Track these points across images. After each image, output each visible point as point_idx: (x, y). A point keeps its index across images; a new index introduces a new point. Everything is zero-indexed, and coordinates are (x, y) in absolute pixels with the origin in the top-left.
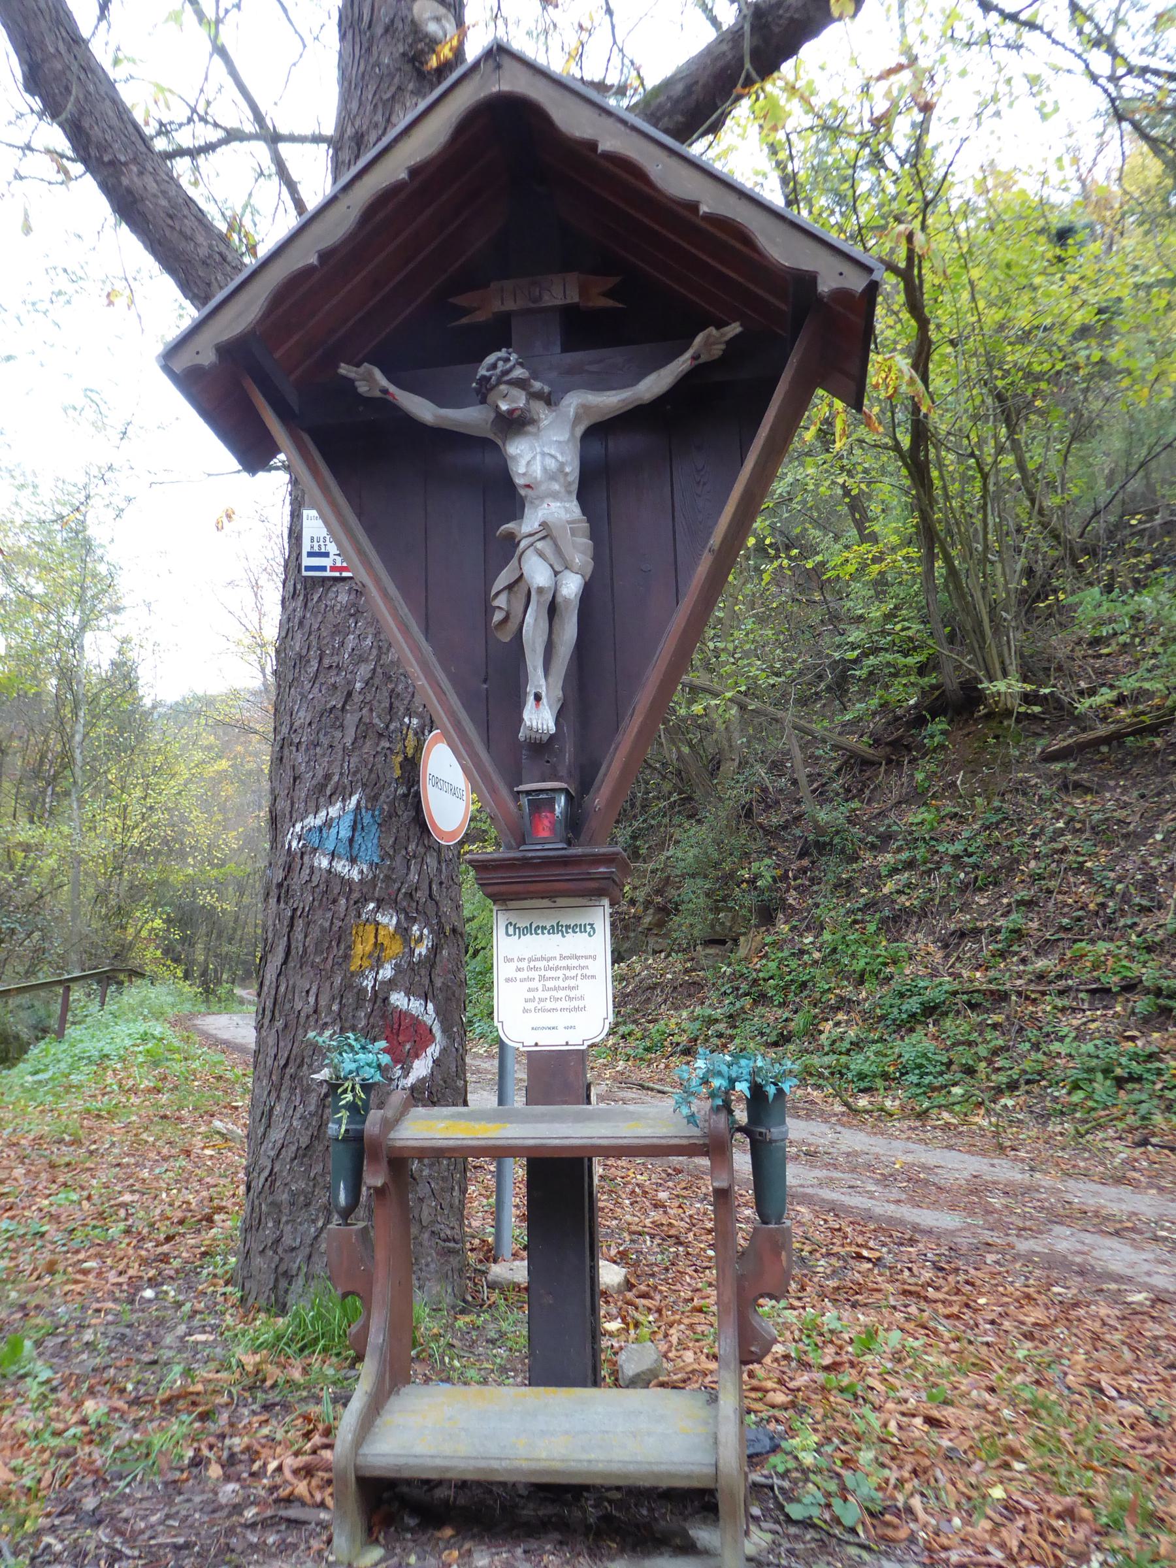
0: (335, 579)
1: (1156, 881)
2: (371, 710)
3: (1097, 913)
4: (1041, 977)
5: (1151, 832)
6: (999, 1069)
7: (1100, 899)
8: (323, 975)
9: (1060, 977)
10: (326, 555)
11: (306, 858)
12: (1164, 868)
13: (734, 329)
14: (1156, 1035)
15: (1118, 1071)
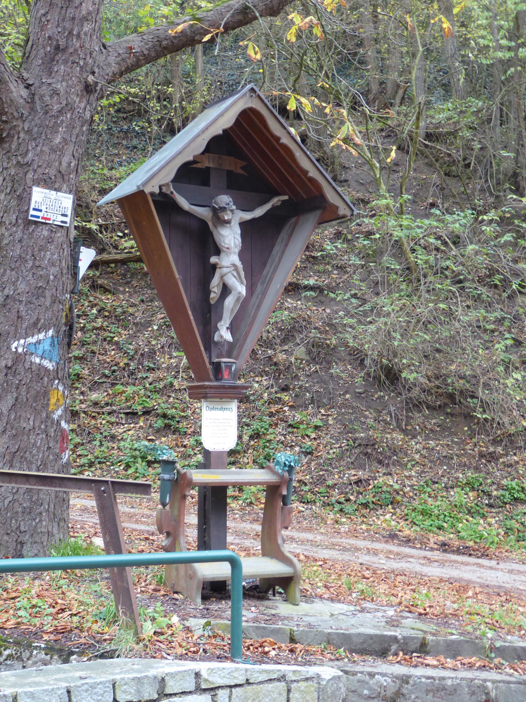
0: (42, 223)
1: (155, 353)
2: (56, 290)
3: (124, 369)
4: (96, 404)
5: (150, 323)
6: (80, 455)
7: (126, 361)
8: (37, 412)
9: (107, 404)
10: (40, 211)
11: (27, 357)
12: (159, 346)
13: (286, 197)
14: (163, 439)
15: (149, 458)
